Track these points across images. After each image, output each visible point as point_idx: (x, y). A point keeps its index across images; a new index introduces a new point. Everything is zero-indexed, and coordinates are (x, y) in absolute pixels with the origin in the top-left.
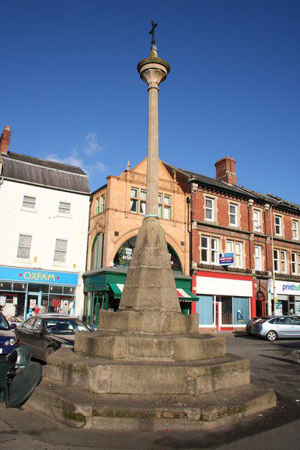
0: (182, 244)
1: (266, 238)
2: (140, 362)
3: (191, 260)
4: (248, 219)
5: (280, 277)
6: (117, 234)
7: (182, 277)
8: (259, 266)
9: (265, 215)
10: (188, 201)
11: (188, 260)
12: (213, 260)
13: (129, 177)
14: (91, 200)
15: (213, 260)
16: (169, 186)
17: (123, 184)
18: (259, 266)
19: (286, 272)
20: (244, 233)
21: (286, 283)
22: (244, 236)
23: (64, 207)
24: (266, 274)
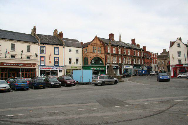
0: (104, 58)
1: (121, 55)
2: (27, 122)
3: (105, 62)
4: (117, 51)
5: (125, 64)
6: (91, 57)
7: (104, 66)
8: (120, 62)
9: (121, 50)
10: (104, 48)
11: (105, 62)
12: (135, 63)
13: (92, 45)
14: (83, 49)
15: (135, 63)
16: (100, 45)
17: (91, 46)
18: (120, 62)
19: (126, 63)
20: (117, 55)
21: (126, 66)
22: (117, 55)
23: (77, 51)
24: (122, 64)
